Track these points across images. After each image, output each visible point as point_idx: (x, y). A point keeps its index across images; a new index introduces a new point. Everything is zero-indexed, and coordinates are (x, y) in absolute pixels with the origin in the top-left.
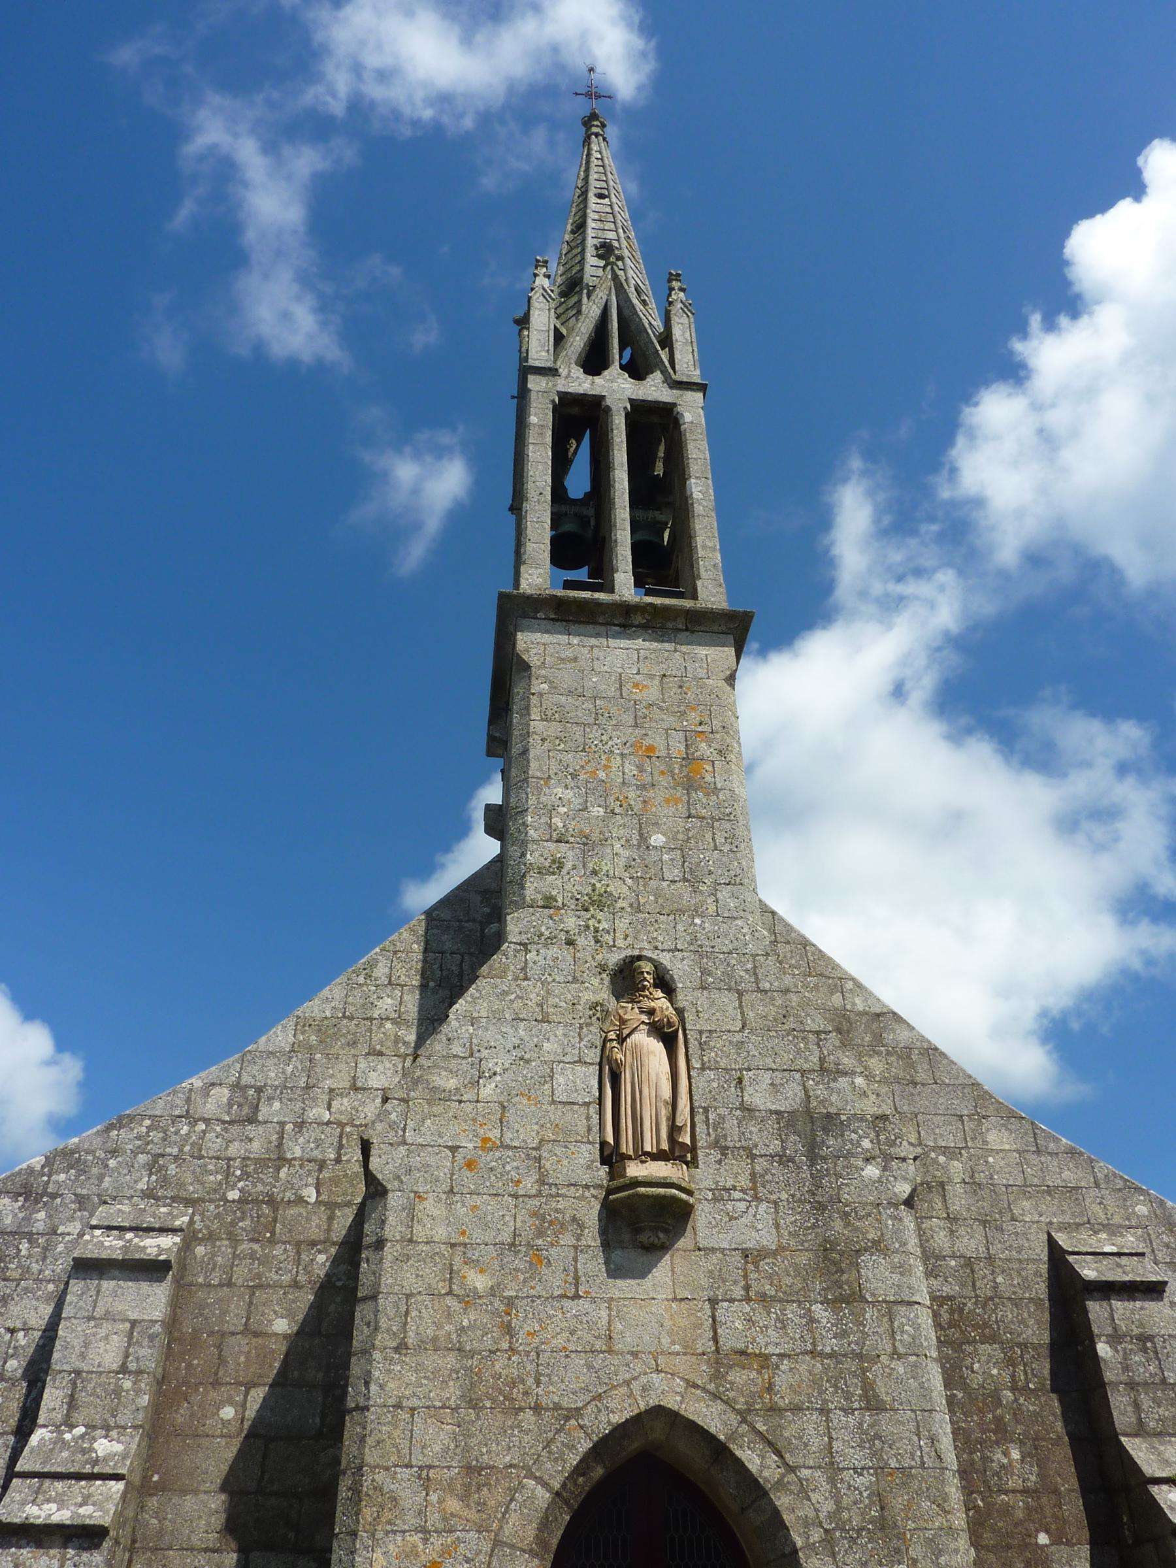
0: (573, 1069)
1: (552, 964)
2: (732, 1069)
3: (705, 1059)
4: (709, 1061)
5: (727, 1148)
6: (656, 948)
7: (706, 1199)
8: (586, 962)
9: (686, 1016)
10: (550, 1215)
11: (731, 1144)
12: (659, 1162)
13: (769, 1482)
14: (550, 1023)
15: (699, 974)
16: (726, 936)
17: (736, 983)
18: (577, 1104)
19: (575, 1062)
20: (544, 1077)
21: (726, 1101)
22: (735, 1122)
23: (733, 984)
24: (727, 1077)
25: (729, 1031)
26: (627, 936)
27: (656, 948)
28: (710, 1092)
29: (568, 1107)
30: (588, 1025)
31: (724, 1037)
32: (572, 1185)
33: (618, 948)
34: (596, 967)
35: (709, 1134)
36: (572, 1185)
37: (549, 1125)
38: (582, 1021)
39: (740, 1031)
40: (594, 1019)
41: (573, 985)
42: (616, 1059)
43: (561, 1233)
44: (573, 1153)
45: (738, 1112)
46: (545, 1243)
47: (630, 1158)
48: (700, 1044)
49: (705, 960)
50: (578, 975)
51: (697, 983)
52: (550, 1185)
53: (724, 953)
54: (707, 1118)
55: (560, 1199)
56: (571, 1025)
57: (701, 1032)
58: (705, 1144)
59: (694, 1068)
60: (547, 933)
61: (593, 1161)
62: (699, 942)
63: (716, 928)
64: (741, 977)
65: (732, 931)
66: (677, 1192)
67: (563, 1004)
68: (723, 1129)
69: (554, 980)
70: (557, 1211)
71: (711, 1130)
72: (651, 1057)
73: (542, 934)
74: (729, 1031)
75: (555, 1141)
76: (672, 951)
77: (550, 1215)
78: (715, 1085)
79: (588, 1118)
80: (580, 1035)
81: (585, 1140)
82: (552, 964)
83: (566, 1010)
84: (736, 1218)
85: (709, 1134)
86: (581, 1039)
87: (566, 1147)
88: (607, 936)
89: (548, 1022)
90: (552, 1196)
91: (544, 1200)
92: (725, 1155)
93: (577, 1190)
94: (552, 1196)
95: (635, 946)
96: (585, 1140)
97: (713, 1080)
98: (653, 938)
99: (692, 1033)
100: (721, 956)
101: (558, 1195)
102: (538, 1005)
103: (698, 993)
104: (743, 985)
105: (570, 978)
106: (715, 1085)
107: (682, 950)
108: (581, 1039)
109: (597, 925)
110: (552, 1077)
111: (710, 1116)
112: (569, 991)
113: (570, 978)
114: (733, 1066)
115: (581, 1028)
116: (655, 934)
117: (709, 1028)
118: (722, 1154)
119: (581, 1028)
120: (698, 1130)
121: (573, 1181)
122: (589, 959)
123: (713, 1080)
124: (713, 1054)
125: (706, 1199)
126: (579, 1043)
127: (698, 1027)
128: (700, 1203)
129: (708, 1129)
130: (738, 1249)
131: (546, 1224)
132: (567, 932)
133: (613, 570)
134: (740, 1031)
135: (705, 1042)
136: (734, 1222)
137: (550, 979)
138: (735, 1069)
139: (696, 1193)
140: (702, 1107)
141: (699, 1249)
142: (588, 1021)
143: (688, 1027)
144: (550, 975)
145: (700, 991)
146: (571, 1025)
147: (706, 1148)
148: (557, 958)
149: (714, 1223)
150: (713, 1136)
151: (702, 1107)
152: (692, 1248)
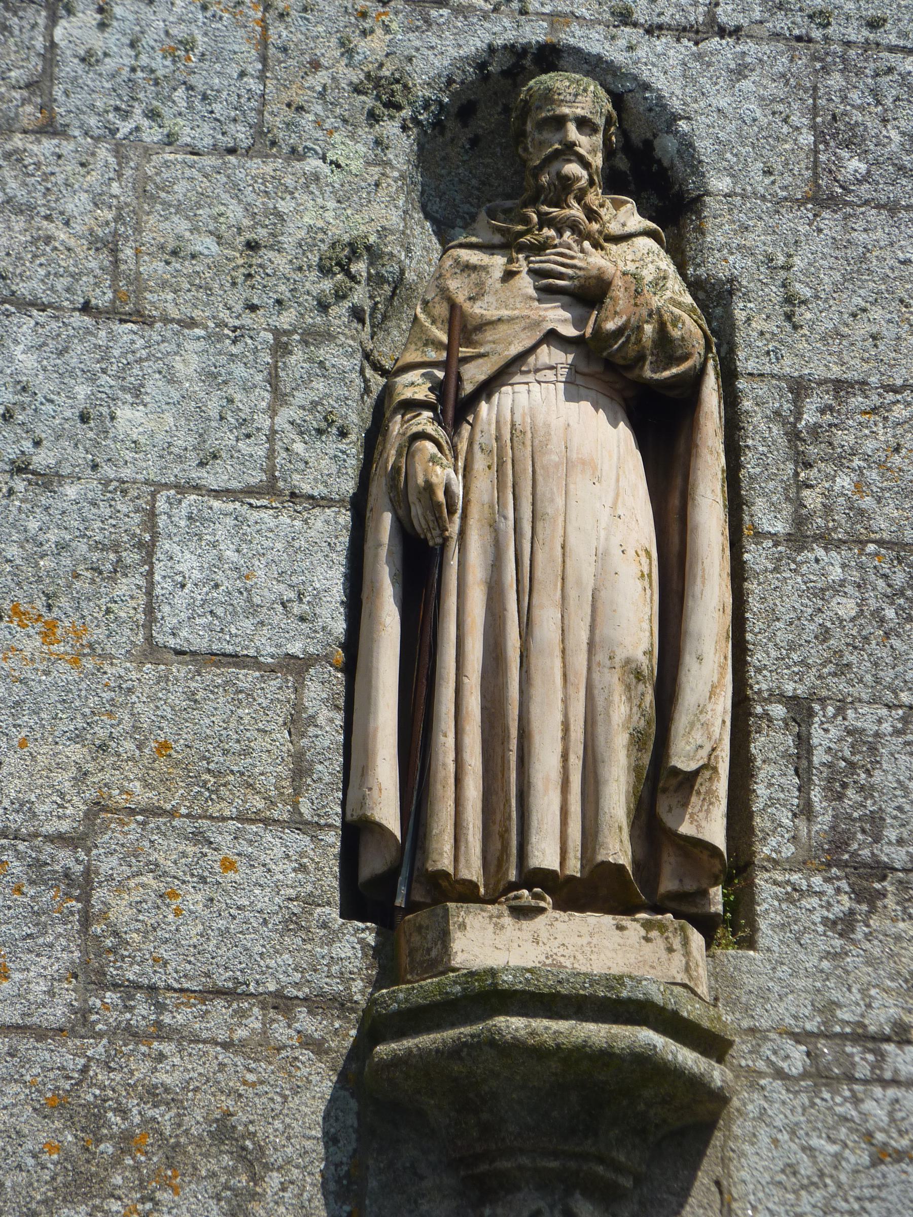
12: (594, 919)
35: (806, 811)
54: (803, 742)
61: (311, 901)
85: (806, 811)
105: (241, 134)
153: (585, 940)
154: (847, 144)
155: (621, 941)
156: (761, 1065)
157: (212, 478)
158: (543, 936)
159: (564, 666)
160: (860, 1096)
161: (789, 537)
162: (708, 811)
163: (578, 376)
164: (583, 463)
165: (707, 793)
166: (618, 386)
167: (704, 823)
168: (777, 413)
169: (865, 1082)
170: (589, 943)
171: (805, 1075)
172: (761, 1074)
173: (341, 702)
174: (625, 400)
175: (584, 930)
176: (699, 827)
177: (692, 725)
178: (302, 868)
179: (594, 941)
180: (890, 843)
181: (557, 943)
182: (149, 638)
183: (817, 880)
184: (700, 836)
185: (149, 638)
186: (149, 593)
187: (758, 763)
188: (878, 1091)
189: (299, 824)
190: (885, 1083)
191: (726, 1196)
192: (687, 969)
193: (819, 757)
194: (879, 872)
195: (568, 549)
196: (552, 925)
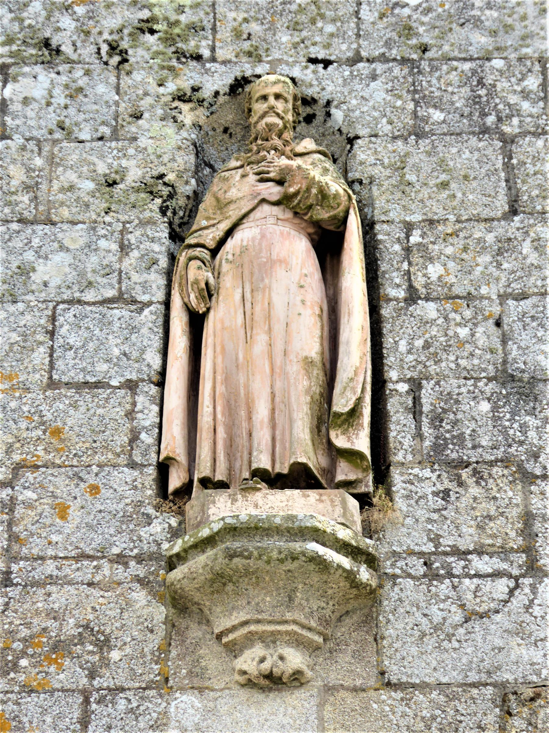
7: (409, 576)
12: (288, 492)
23: (491, 120)
35: (419, 435)
54: (416, 400)
57: (409, 228)
61: (140, 504)
85: (419, 435)
105: (106, 131)
136: (477, 625)
153: (284, 504)
154: (435, 107)
155: (305, 503)
156: (398, 571)
157: (90, 296)
158: (260, 503)
159: (272, 364)
160: (456, 584)
161: (406, 300)
162: (357, 434)
163: (279, 221)
164: (280, 261)
165: (356, 425)
166: (302, 226)
167: (355, 441)
168: (398, 239)
169: (458, 577)
170: (287, 505)
171: (425, 576)
172: (398, 577)
173: (158, 401)
174: (309, 235)
175: (284, 498)
176: (352, 443)
177: (345, 388)
178: (135, 488)
179: (290, 504)
180: (469, 449)
181: (268, 507)
182: (51, 378)
183: (427, 473)
184: (353, 447)
185: (51, 378)
186: (51, 356)
187: (392, 414)
188: (467, 581)
189: (132, 465)
190: (471, 577)
191: (380, 646)
192: (344, 515)
193: (426, 408)
194: (12, 55)
195: (271, 305)
196: (265, 497)
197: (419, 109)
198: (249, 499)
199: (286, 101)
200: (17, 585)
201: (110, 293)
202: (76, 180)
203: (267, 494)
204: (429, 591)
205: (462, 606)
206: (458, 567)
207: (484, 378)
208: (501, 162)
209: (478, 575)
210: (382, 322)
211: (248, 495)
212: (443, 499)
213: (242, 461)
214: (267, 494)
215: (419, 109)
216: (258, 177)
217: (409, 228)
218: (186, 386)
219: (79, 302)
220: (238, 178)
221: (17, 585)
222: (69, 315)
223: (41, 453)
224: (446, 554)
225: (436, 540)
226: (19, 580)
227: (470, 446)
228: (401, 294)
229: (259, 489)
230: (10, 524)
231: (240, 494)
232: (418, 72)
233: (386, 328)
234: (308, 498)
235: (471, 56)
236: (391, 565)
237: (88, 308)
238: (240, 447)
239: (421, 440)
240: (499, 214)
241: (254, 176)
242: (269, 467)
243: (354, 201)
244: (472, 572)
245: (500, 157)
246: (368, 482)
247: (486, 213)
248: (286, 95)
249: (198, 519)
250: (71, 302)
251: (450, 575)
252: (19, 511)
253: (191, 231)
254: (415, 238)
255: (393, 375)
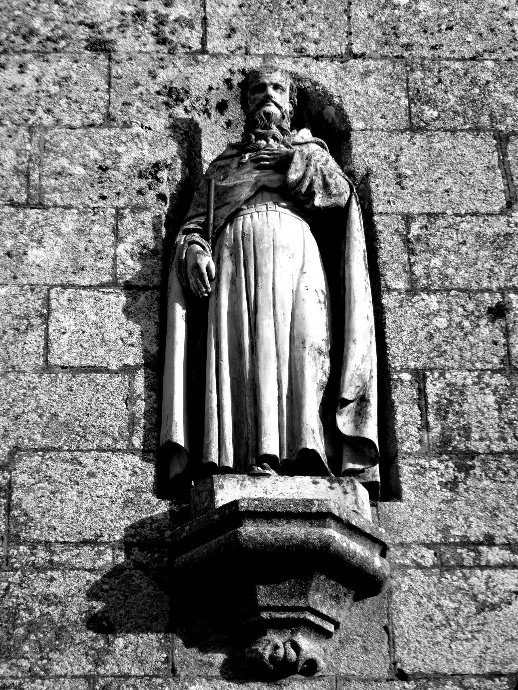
0: (97, 300)
1: (54, 89)
2: (482, 291)
3: (419, 270)
4: (428, 276)
5: (473, 455)
6: (301, 52)
7: (419, 566)
8: (137, 84)
9: (373, 185)
10: (30, 610)
11: (482, 447)
12: (298, 479)
13: (57, 291)
14: (46, 208)
15: (405, 102)
16: (468, 26)
17: (492, 117)
18: (107, 370)
19: (103, 285)
20: (27, 317)
21: (468, 355)
22: (491, 399)
23: (485, 120)
24: (471, 306)
25: (476, 214)
26: (233, 30)
27: (301, 52)
28: (430, 337)
29: (82, 378)
30: (136, 209)
31: (464, 226)
32: (86, 542)
33: (214, 55)
34: (158, 93)
35: (426, 427)
36: (86, 542)
37: (34, 416)
38: (122, 202)
39: (502, 213)
40: (152, 195)
41: (105, 132)
42: (197, 267)
43: (57, 649)
44: (92, 475)
45: (498, 379)
46: (15, 672)
47: (225, 471)
48: (407, 241)
49: (418, 75)
50: (116, 110)
51: (403, 120)
52: (34, 545)
53: (463, 59)
54: (422, 392)
55: (56, 574)
56: (95, 211)
57: (408, 219)
58: (417, 448)
59: (390, 290)
60: (45, 31)
61: (139, 491)
62: (404, 40)
63: (445, 10)
64: (505, 106)
65: (481, 18)
66: (337, 536)
67: (79, 171)
68: (460, 414)
69: (58, 121)
70: (46, 599)
71: (431, 418)
72: (282, 257)
73: (33, 32)
74: (476, 214)
75: (46, 449)
76: (342, 59)
77: (30, 610)
78: (441, 322)
79: (129, 400)
80: (115, 231)
81: (122, 445)
82: (54, 89)
83: (84, 181)
84: (493, 607)
85: (426, 427)
86: (118, 239)
87: (74, 461)
88: (187, 33)
89: (42, 206)
90: (36, 568)
91: (16, 577)
92: (467, 470)
93: (100, 553)
94: (36, 568)
95: (253, 50)
96: (122, 445)
97: (436, 313)
98: (295, 35)
99: (387, 220)
100: (457, 65)
101: (52, 565)
102: (17, 172)
103: (404, 140)
104: (509, 120)
105: (96, 117)
106: (441, 322)
107: (362, 56)
108: (118, 239)
109: (163, 10)
110: (46, 318)
111: (430, 389)
112: (94, 145)
113: (96, 117)
114: (485, 284)
115: (119, 215)
116: (300, 26)
117: (427, 209)
118: (459, 468)
119: (119, 215)
120: (400, 419)
121: (88, 535)
122: (144, 78)
123: (436, 313)
124: (436, 262)
125: (419, 566)
126: (115, 246)
127: (401, 207)
128: (404, 574)
129: (424, 414)
130: (499, 675)
131: (21, 631)
132: (91, 26)
133: (354, 463)
134: (502, 213)
135: (418, 238)
136: (490, 615)
137: (48, 120)
138: (489, 290)
139: (393, 552)
140: (408, 370)
141: (402, 676)
142: (139, 200)
143: (378, 207)
144: (48, 111)
145: (407, 135)
146: (95, 211)
147: (419, 455)
148: (66, 79)
149: (438, 617)
150: (436, 430)
151: (408, 370)
152: (384, 673)
155: (316, 490)
156: (407, 562)
157: (85, 279)
161: (407, 291)
169: (470, 567)
170: (297, 492)
171: (434, 566)
175: (294, 485)
179: (300, 491)
180: (476, 440)
181: (278, 493)
182: (46, 361)
183: (435, 463)
188: (479, 572)
190: (482, 568)
196: (274, 483)
197: (413, 105)
198: (258, 485)
199: (283, 90)
200: (17, 570)
201: (106, 278)
202: (67, 166)
203: (277, 480)
204: (440, 582)
205: (474, 597)
206: (468, 557)
207: (489, 370)
208: (496, 159)
209: (488, 566)
210: (384, 313)
211: (256, 480)
212: (451, 490)
213: (248, 449)
214: (277, 480)
215: (413, 105)
216: (256, 165)
217: (408, 219)
218: (350, 280)
219: (73, 286)
220: (234, 165)
221: (17, 570)
222: (63, 299)
223: (38, 437)
224: (455, 544)
225: (446, 530)
226: (17, 565)
227: (477, 437)
228: (401, 285)
229: (269, 475)
230: (9, 508)
231: (249, 480)
232: (411, 70)
233: (389, 319)
234: (318, 485)
235: (462, 57)
236: (401, 555)
237: (83, 292)
238: (245, 433)
239: (428, 431)
240: (497, 209)
241: (252, 164)
242: (277, 454)
243: (355, 191)
244: (483, 563)
245: (496, 154)
246: (375, 471)
247: (484, 208)
248: (283, 84)
249: (206, 505)
250: (64, 287)
251: (461, 566)
252: (16, 495)
253: (186, 218)
254: (415, 230)
255: (396, 364)
